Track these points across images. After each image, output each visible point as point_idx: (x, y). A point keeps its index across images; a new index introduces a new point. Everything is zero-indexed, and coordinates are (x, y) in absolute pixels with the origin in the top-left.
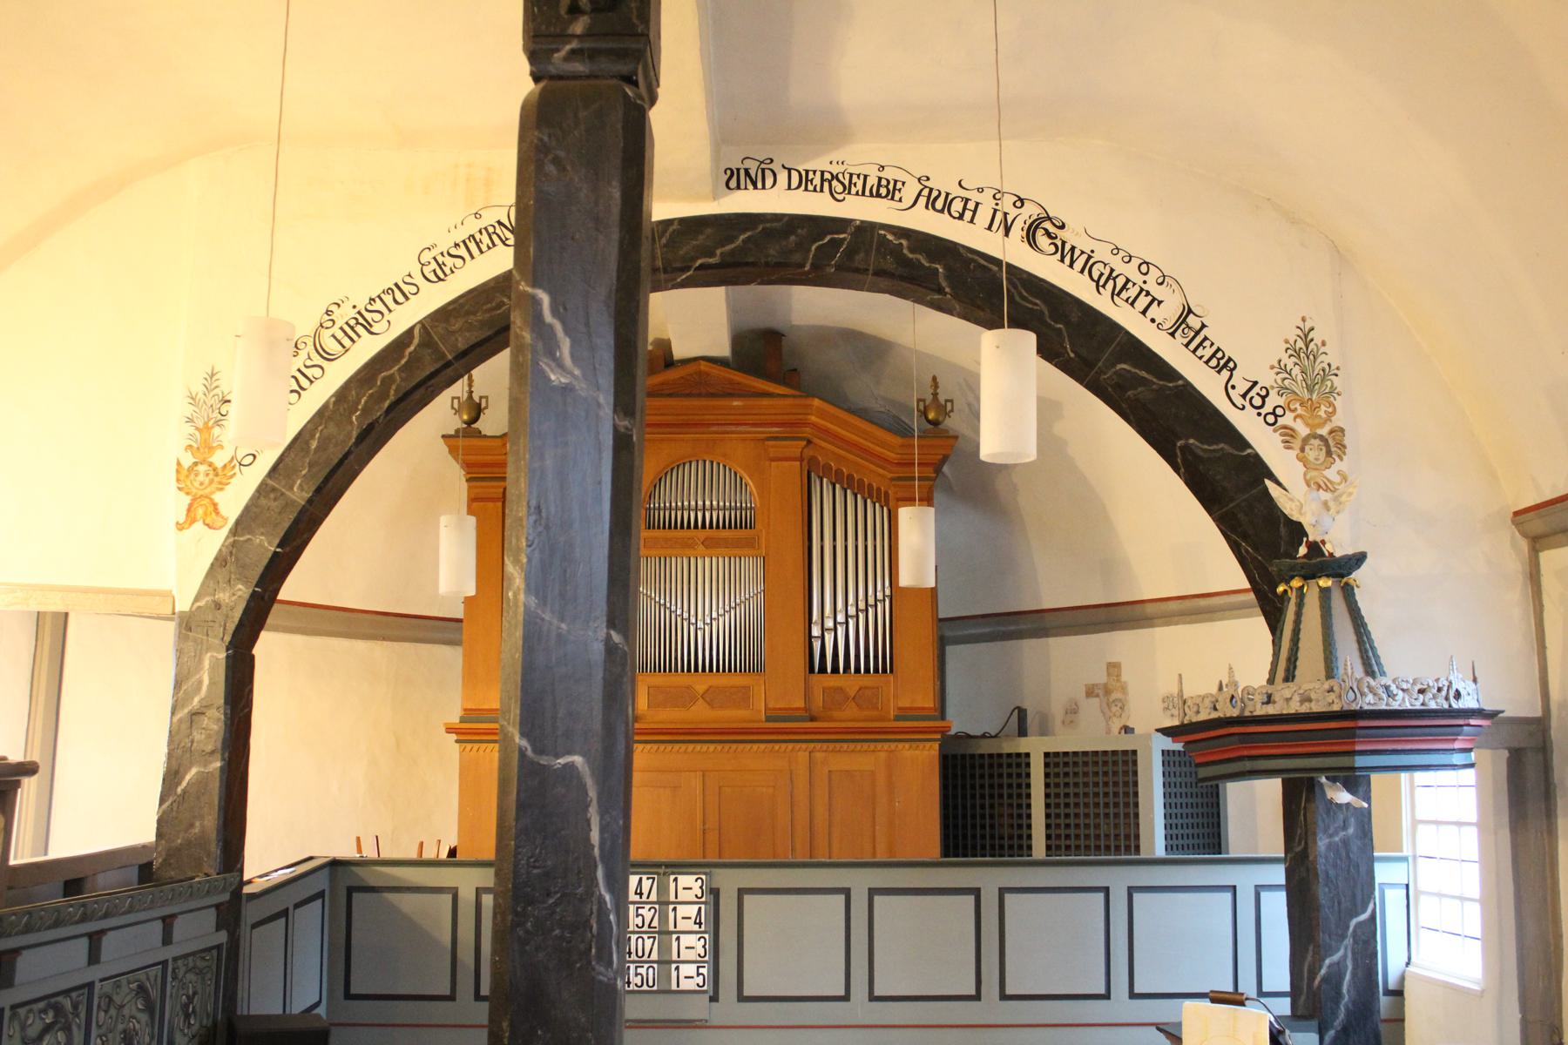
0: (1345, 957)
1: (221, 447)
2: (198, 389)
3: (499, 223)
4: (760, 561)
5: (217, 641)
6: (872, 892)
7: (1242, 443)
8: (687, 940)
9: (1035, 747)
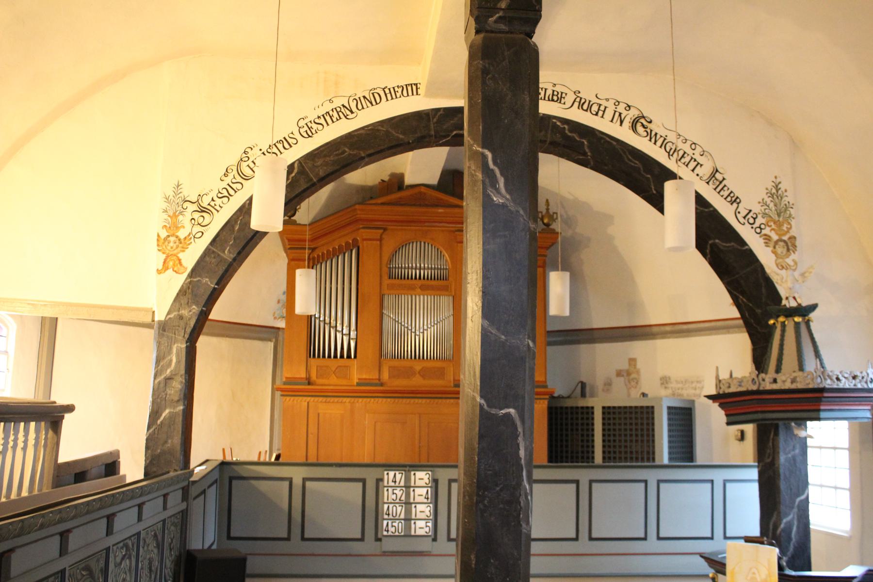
0: (793, 518)
1: (184, 227)
3: (344, 106)
4: (451, 298)
5: (181, 338)
7: (743, 243)
8: (420, 507)
9: (597, 403)
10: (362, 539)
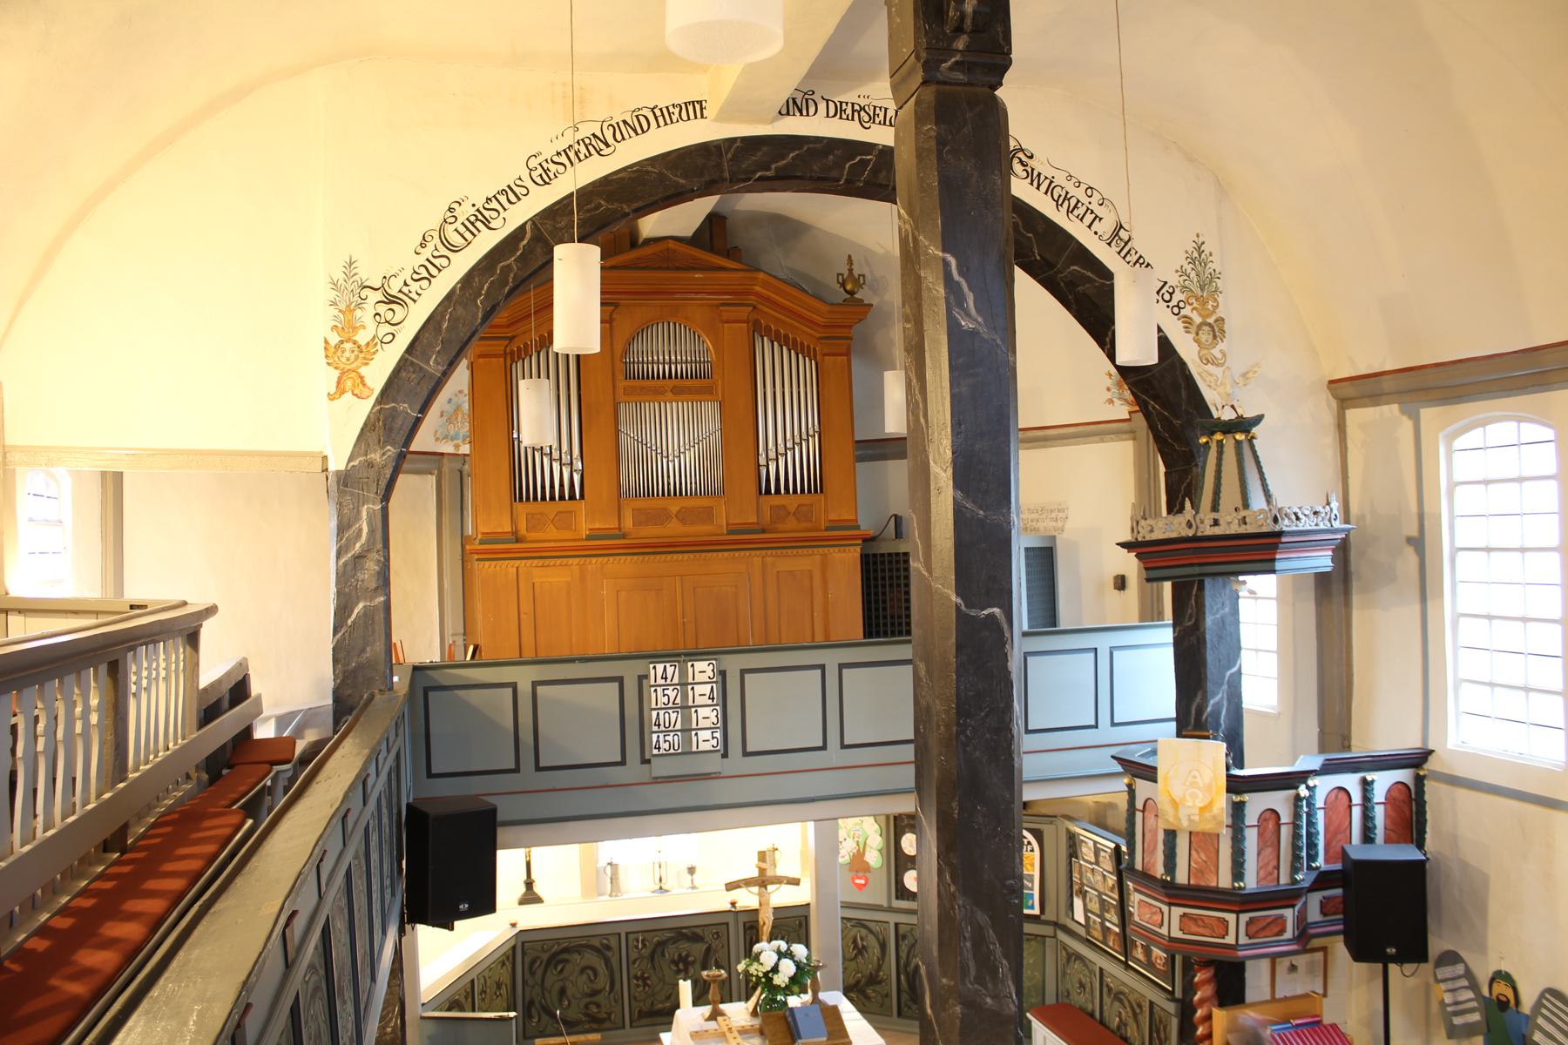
2: (339, 275)
4: (717, 405)
6: (841, 666)
8: (703, 712)
10: (623, 763)
